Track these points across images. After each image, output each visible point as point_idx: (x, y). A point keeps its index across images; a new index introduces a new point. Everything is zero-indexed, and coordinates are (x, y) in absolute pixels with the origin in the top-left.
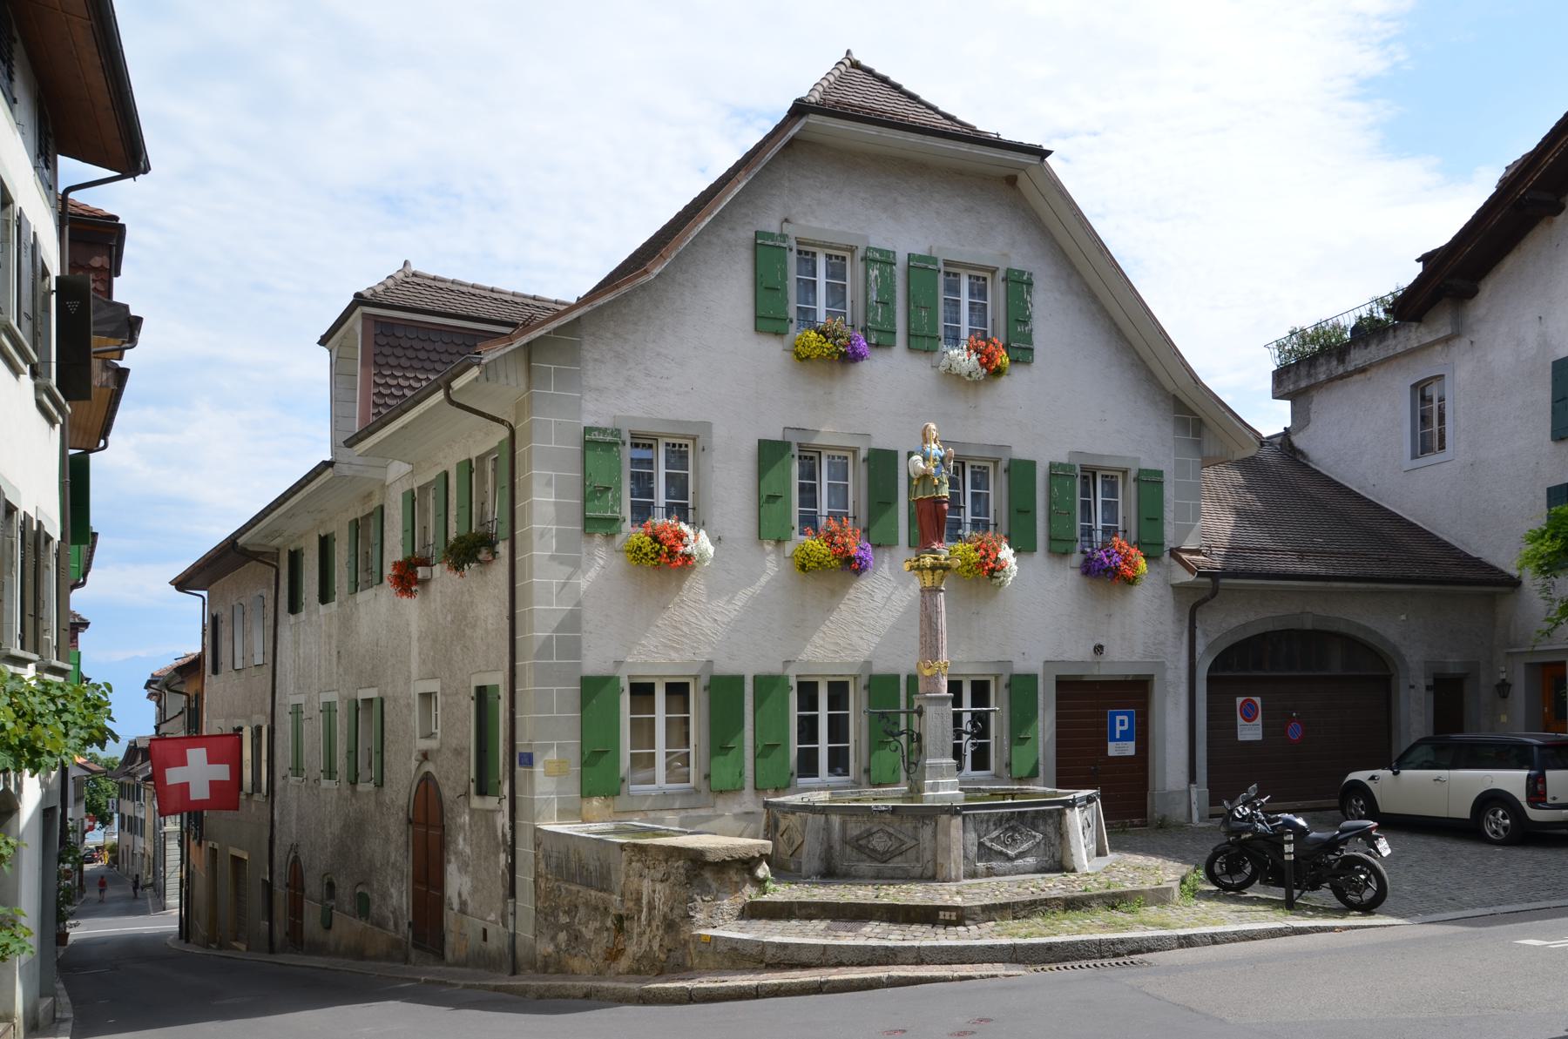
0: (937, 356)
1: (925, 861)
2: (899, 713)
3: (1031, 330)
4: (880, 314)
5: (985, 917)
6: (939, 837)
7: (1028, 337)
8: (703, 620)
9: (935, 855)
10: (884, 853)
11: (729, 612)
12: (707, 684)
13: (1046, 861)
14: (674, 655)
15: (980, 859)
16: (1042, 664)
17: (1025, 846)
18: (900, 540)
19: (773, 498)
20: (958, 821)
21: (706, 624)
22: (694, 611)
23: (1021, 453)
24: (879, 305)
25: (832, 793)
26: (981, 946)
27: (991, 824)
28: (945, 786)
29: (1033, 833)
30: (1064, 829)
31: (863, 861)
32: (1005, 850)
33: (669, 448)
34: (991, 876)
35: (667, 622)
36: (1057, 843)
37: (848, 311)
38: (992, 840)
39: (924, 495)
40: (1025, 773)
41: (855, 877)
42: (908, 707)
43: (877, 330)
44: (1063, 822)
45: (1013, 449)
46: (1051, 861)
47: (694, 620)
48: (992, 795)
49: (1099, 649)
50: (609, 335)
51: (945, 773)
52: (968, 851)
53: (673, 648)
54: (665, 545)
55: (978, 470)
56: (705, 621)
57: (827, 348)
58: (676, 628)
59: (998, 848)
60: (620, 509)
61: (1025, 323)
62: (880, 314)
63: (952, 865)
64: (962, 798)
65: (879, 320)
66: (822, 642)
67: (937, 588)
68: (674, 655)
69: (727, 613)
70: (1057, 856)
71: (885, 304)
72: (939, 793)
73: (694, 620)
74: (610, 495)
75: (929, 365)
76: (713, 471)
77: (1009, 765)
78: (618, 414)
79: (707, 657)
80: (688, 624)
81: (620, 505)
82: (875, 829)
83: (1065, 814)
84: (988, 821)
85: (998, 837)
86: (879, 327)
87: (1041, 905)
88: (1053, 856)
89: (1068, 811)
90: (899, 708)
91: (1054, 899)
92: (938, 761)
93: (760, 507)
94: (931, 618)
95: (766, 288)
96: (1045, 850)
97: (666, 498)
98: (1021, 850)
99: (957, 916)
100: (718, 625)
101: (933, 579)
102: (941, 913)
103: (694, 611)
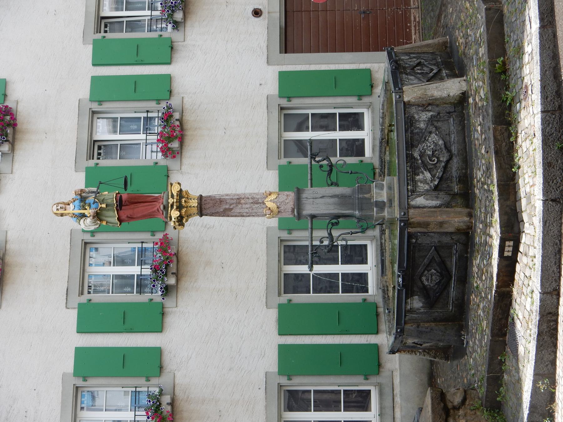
1: (452, 241)
2: (312, 246)
9: (446, 233)
10: (441, 275)
16: (270, 67)
18: (152, 345)
23: (85, 91)
36: (437, 109)
41: (463, 299)
42: (306, 229)
45: (81, 97)
49: (257, 13)
70: (449, 108)
90: (307, 246)
96: (443, 121)
97: (135, 265)
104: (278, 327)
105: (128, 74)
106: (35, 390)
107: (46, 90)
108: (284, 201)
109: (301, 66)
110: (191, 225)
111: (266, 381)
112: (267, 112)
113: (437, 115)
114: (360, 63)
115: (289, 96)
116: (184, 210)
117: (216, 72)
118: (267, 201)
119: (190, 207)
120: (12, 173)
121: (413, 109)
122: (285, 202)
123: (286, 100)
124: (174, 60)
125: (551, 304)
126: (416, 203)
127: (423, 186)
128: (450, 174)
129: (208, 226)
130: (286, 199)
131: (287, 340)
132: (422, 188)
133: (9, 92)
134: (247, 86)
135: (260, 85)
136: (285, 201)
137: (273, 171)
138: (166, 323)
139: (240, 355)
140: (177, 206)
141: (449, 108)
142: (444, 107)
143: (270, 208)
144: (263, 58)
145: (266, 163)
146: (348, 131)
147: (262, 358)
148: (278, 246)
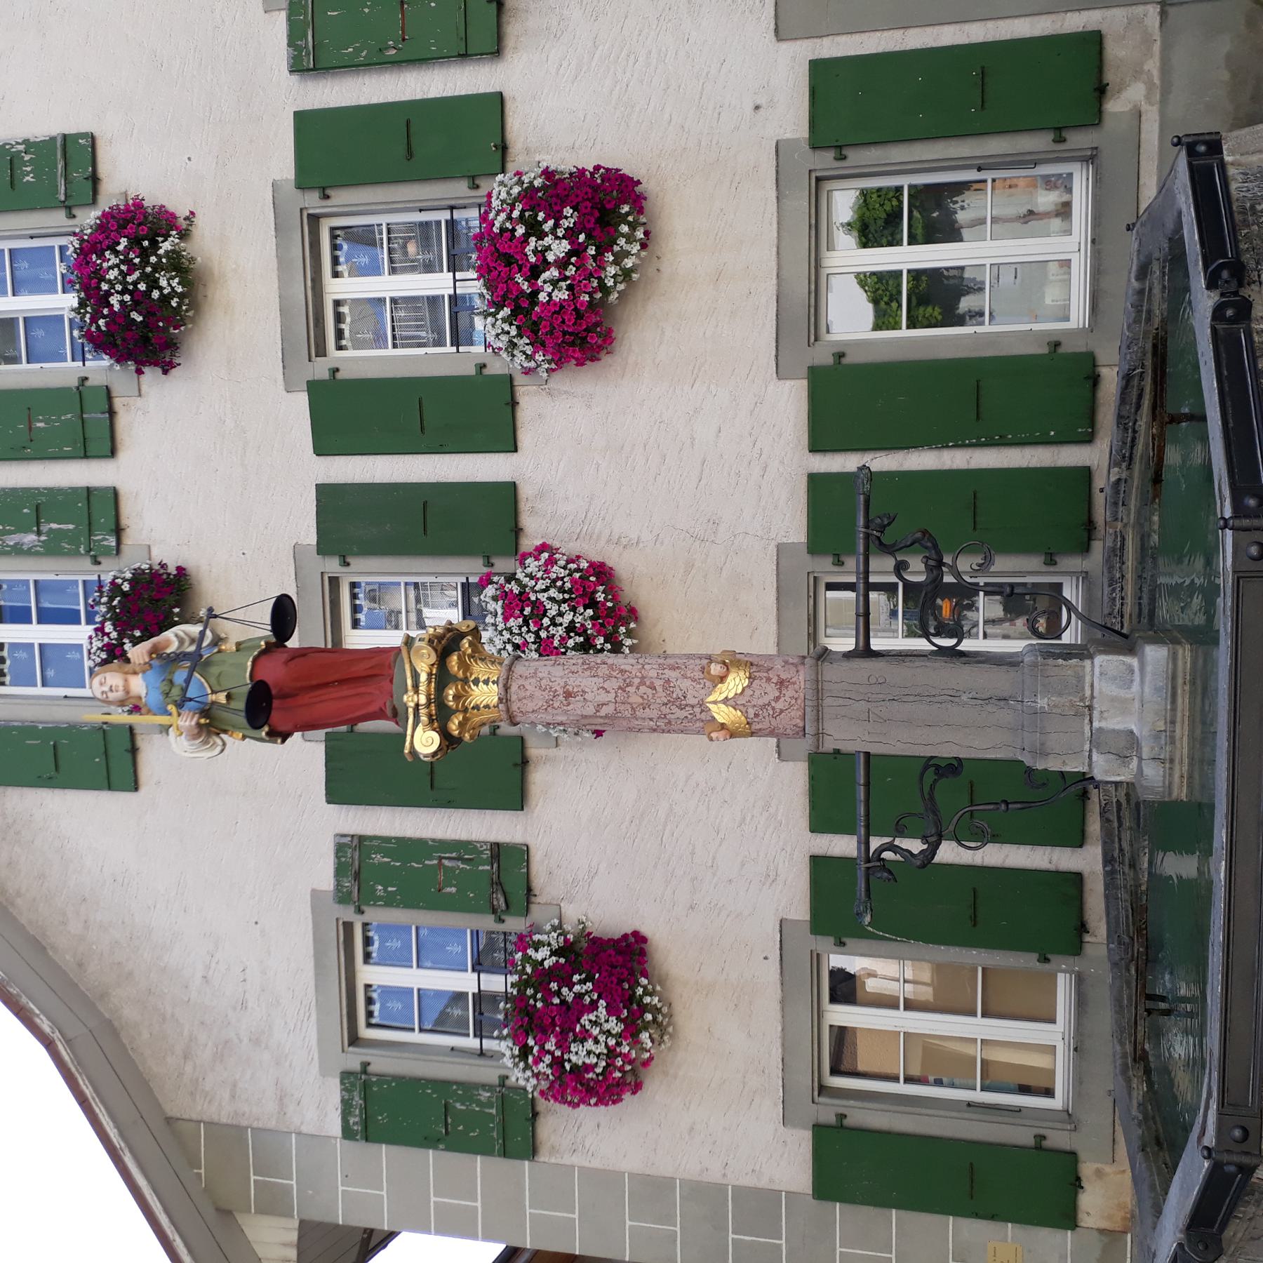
16: (784, 46)
106: (256, 923)
108: (769, 704)
109: (878, 34)
110: (581, 536)
111: (781, 941)
112: (778, 198)
115: (839, 144)
116: (457, 722)
117: (628, 74)
118: (715, 702)
119: (477, 707)
120: (140, 395)
122: (773, 709)
123: (830, 155)
124: (510, 42)
129: (624, 541)
130: (777, 699)
131: (833, 845)
133: (103, 170)
134: (716, 115)
136: (773, 704)
137: (792, 382)
138: (534, 783)
139: (714, 874)
140: (430, 716)
143: (723, 725)
144: (763, 18)
145: (773, 358)
147: (771, 884)
148: (809, 597)
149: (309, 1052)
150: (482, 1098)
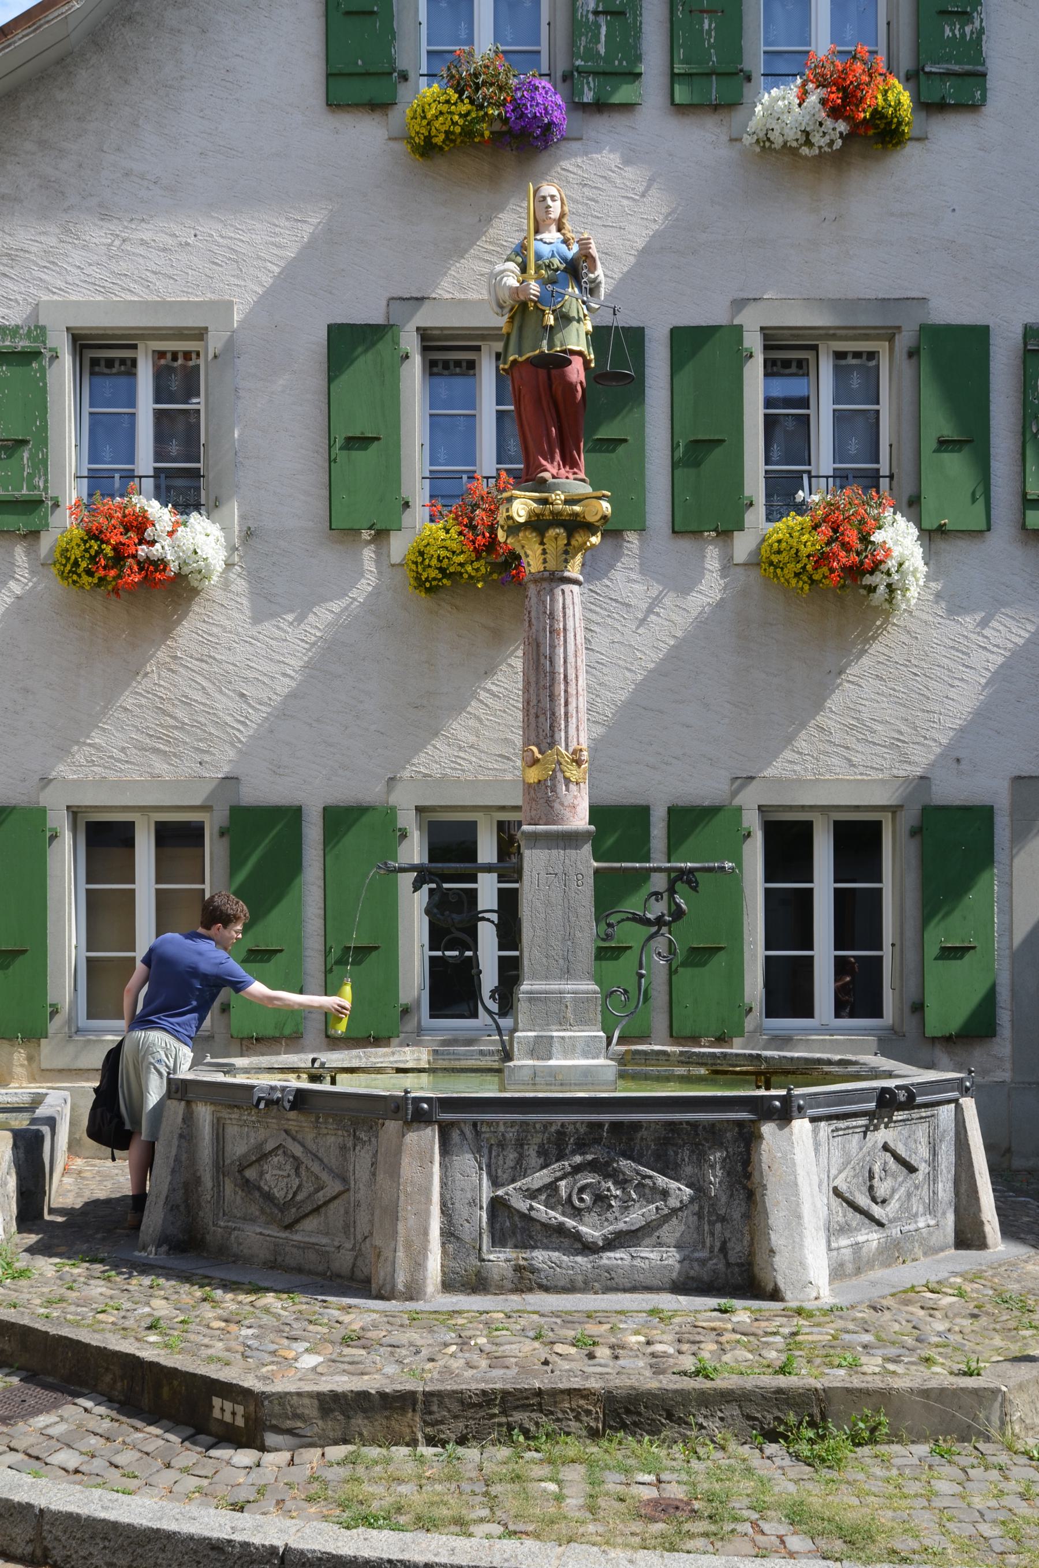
0: (739, 115)
1: (359, 1237)
3: (981, 31)
4: (603, 39)
5: (331, 1427)
6: (380, 1177)
7: (974, 47)
8: (218, 696)
11: (272, 678)
12: (225, 823)
13: (703, 1262)
14: (160, 766)
15: (499, 1240)
17: (637, 1216)
19: (358, 442)
20: (431, 1135)
21: (224, 703)
22: (199, 679)
24: (602, 20)
25: (436, 1052)
26: (191, 1538)
27: (532, 1152)
28: (569, 1048)
29: (662, 1181)
30: (756, 1178)
31: (253, 1220)
32: (570, 1223)
33: (163, 362)
34: (530, 1290)
35: (143, 701)
36: (736, 1215)
37: (544, 48)
38: (532, 1194)
39: (520, 355)
40: (954, 1025)
43: (596, 74)
44: (754, 1157)
45: (933, 304)
46: (717, 1263)
47: (198, 696)
48: (716, 1072)
50: (29, 146)
51: (570, 1015)
52: (457, 1220)
53: (156, 751)
54: (108, 543)
55: (855, 362)
56: (224, 699)
57: (461, 115)
58: (164, 712)
59: (556, 1216)
60: (46, 481)
61: (965, 16)
62: (603, 39)
63: (401, 1254)
64: (611, 1074)
65: (602, 51)
66: (472, 739)
67: (553, 573)
68: (160, 766)
69: (266, 680)
70: (737, 1250)
71: (616, 14)
72: (552, 1062)
73: (198, 696)
74: (26, 455)
75: (725, 138)
76: (238, 398)
77: (918, 1008)
78: (45, 298)
79: (225, 770)
80: (187, 703)
81: (46, 474)
82: (269, 1146)
83: (760, 1137)
84: (520, 1144)
85: (551, 1188)
86: (602, 66)
87: (525, 1407)
88: (723, 1249)
89: (768, 1129)
91: (570, 1392)
92: (554, 986)
93: (331, 461)
94: (538, 646)
95: (348, 13)
98: (621, 1226)
99: (246, 1417)
100: (249, 705)
101: (544, 552)
102: (217, 1402)
103: (199, 679)
104: (342, 804)
105: (991, 422)
107: (954, 210)
113: (718, 1215)
114: (1011, 1011)
121: (738, 1147)
125: (14, 1535)
126: (456, 1145)
127: (506, 1166)
128: (541, 1241)
132: (501, 1162)
135: (958, 760)
141: (737, 1250)
142: (743, 1234)
146: (498, 936)
149: (60, 289)
150: (37, 479)
